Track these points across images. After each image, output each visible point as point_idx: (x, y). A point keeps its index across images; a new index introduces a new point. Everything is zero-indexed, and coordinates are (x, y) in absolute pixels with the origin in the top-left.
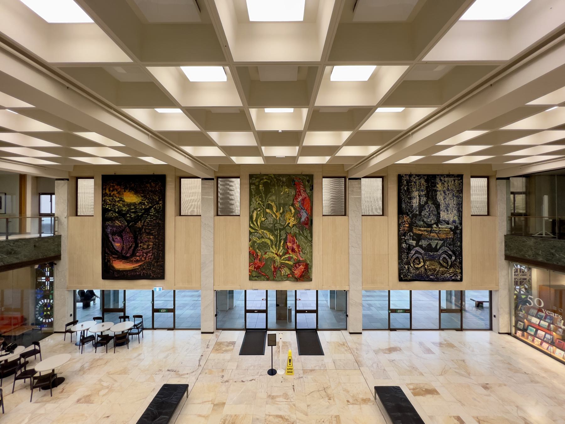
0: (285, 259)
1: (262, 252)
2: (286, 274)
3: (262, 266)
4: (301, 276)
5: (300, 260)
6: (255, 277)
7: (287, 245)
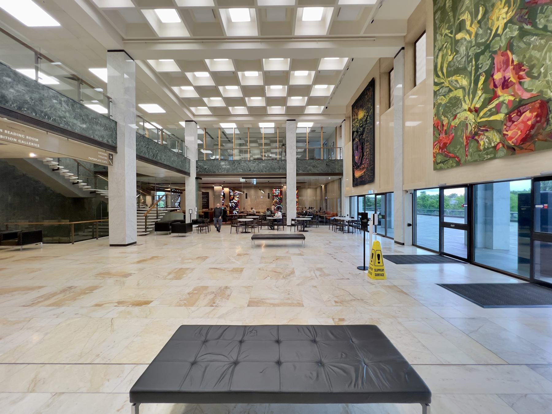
0: (489, 113)
1: (449, 117)
2: (493, 145)
3: (448, 142)
4: (524, 140)
5: (521, 100)
6: (441, 162)
7: (494, 79)
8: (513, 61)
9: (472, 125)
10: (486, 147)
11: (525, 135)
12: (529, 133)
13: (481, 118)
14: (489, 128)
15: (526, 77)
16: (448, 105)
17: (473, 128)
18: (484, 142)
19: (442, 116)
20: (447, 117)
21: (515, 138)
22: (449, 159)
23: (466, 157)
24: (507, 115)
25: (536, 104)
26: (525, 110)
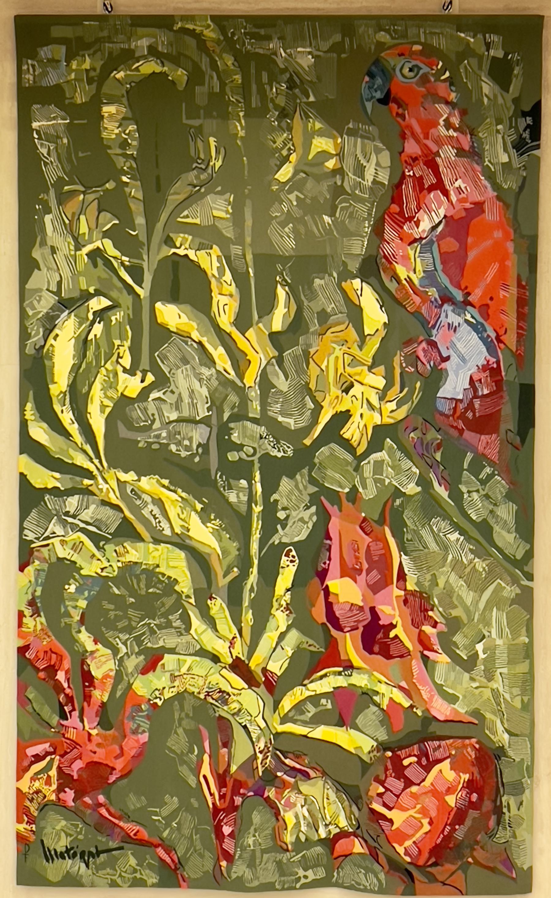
3: (119, 764)
7: (327, 590)
8: (402, 576)
9: (254, 736)
10: (303, 838)
11: (442, 836)
12: (450, 832)
13: (284, 720)
14: (312, 768)
15: (440, 651)
16: (117, 591)
17: (261, 752)
18: (297, 817)
19: (83, 629)
20: (115, 651)
21: (414, 839)
22: (121, 848)
23: (224, 863)
24: (385, 750)
25: (465, 746)
26: (438, 755)
